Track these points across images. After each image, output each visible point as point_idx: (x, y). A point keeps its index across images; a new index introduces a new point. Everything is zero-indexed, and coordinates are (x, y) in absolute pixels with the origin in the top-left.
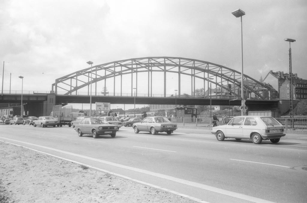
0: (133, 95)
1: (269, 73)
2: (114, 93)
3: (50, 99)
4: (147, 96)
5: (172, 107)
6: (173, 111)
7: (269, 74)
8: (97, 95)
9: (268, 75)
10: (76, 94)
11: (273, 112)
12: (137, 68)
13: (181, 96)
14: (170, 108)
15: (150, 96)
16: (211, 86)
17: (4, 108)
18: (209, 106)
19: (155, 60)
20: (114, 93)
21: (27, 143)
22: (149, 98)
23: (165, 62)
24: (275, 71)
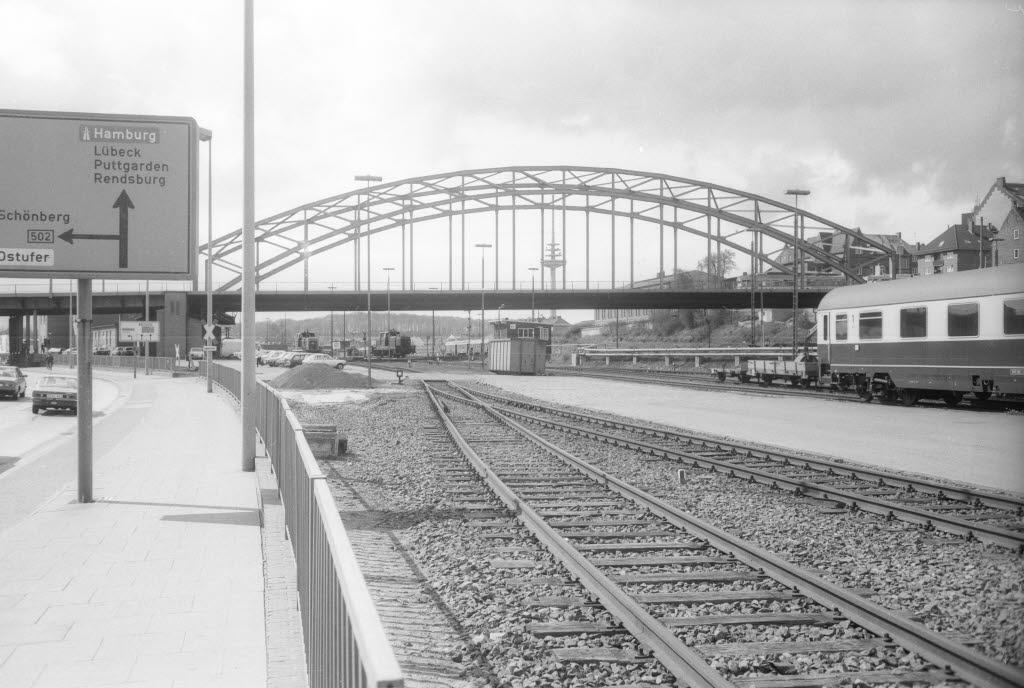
0: (364, 288)
1: (995, 185)
2: (613, 282)
3: (172, 304)
4: (446, 287)
5: (642, 315)
6: (647, 325)
7: (992, 190)
8: (54, 291)
9: (989, 194)
10: (611, 288)
11: (517, 343)
12: (449, 202)
13: (635, 286)
14: (638, 319)
15: (408, 288)
16: (380, 230)
17: (105, 328)
18: (747, 311)
19: (537, 176)
20: (613, 282)
21: (398, 391)
22: (661, 293)
23: (662, 193)
24: (1008, 181)
